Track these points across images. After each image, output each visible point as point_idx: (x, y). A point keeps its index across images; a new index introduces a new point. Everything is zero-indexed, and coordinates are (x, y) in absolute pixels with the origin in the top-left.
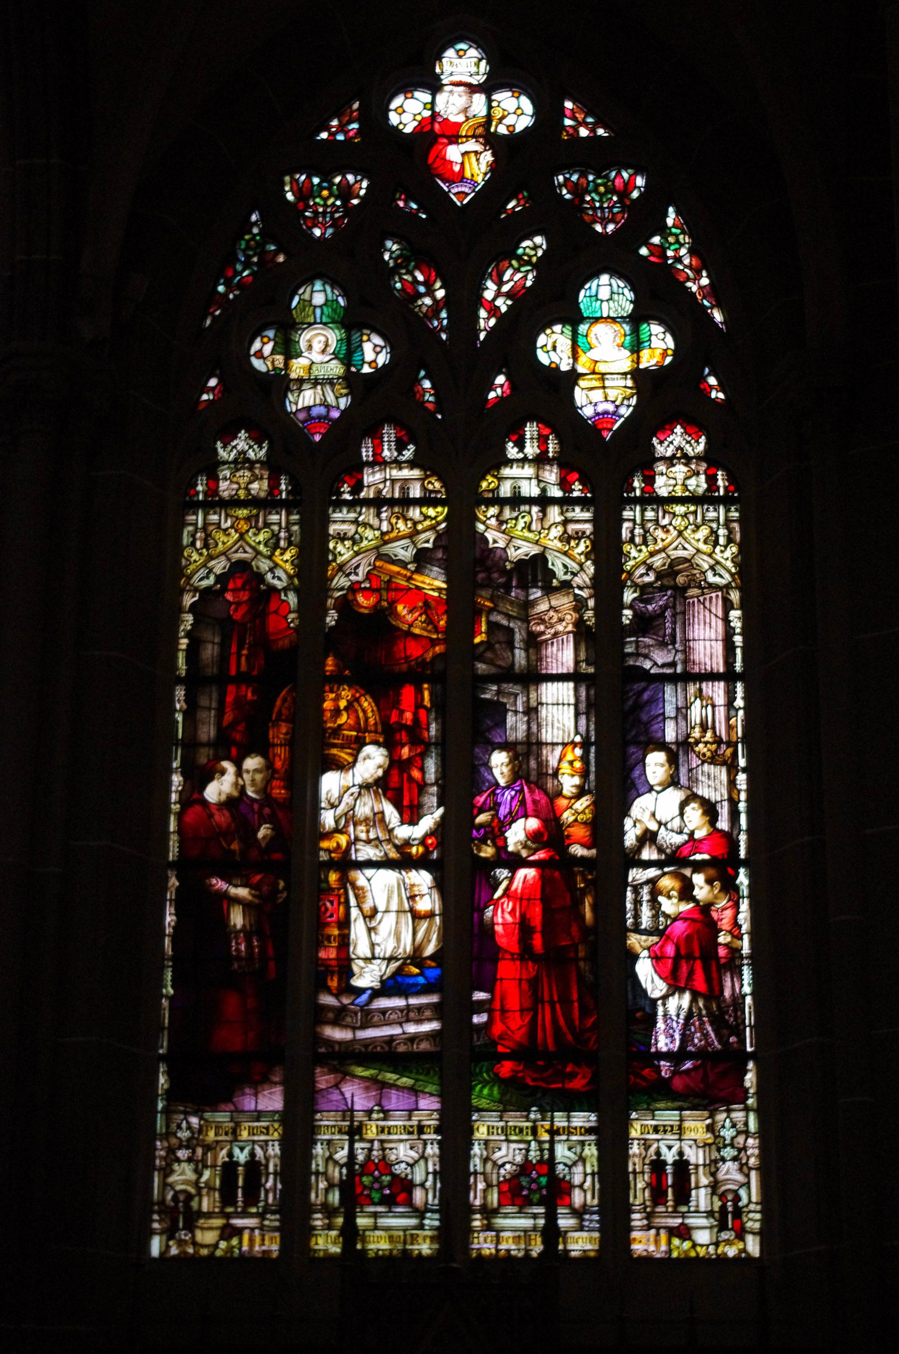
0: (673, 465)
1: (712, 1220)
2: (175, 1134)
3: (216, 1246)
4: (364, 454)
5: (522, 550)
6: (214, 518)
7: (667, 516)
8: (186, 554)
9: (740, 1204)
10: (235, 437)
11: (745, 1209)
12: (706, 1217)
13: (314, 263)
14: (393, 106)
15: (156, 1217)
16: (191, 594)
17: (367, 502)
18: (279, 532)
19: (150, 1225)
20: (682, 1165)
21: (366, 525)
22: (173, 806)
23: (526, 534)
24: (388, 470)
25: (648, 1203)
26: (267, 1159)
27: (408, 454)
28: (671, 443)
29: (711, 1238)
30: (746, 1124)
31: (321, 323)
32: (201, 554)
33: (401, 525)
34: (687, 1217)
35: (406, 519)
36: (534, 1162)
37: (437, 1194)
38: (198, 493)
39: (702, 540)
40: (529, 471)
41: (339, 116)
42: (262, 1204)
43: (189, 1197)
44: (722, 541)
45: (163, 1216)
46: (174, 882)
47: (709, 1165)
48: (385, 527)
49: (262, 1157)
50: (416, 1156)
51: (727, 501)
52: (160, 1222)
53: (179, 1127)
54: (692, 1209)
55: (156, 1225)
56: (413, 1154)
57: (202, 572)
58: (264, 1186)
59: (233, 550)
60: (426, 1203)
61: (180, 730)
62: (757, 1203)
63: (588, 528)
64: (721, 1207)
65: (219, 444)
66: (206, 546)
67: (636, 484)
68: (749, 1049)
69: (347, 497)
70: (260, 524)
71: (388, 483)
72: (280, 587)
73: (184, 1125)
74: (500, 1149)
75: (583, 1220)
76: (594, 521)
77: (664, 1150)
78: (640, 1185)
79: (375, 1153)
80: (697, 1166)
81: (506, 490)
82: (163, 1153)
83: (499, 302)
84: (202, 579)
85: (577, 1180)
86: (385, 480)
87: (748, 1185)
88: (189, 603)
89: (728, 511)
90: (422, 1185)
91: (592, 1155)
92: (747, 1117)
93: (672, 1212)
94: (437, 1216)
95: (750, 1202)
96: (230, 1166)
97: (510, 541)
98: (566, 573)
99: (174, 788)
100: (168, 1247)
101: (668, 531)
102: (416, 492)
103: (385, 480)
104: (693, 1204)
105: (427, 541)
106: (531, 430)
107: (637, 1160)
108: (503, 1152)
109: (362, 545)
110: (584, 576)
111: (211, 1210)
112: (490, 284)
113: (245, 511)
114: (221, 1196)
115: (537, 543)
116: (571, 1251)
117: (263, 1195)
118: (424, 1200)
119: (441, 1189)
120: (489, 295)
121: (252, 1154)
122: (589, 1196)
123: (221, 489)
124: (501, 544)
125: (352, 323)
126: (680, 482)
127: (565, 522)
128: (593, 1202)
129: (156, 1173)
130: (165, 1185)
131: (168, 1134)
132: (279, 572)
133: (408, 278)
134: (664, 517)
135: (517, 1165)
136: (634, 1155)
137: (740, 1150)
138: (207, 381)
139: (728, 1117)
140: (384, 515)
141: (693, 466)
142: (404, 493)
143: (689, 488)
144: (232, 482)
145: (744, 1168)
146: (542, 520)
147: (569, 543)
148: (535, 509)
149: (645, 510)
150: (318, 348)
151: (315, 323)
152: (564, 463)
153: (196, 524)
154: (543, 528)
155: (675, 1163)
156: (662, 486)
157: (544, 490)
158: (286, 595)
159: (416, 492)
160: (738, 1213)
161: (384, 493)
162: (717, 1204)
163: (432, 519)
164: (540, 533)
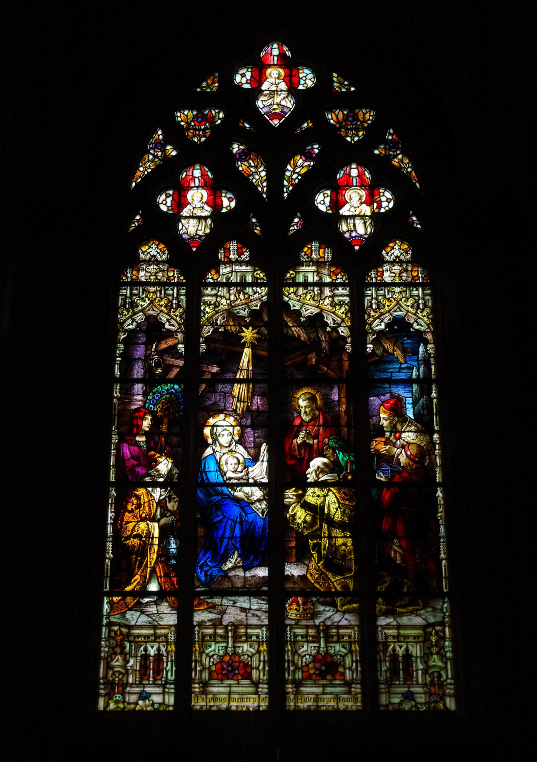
0: (150, 265)
1: (426, 689)
3: (137, 704)
4: (220, 256)
5: (310, 310)
7: (390, 293)
8: (120, 310)
9: (442, 679)
13: (190, 155)
14: (241, 72)
18: (419, 300)
20: (408, 656)
21: (223, 297)
22: (112, 451)
28: (393, 254)
30: (444, 632)
32: (128, 311)
34: (412, 687)
44: (421, 306)
45: (106, 686)
47: (424, 657)
50: (254, 651)
52: (104, 689)
54: (414, 683)
55: (102, 691)
57: (129, 321)
59: (393, 310)
61: (434, 409)
63: (347, 299)
64: (430, 682)
71: (234, 273)
75: (351, 688)
76: (350, 295)
77: (398, 648)
79: (229, 649)
80: (417, 657)
81: (300, 279)
84: (377, 326)
85: (255, 664)
86: (232, 272)
88: (371, 339)
89: (424, 290)
91: (264, 650)
94: (359, 686)
97: (302, 306)
101: (391, 301)
104: (415, 679)
105: (257, 306)
108: (305, 648)
109: (220, 308)
111: (134, 682)
115: (318, 307)
116: (321, 706)
122: (262, 674)
124: (298, 308)
125: (214, 188)
127: (333, 296)
132: (173, 322)
134: (143, 294)
138: (135, 216)
139: (119, 629)
140: (232, 292)
142: (242, 279)
143: (403, 278)
145: (443, 657)
148: (316, 289)
149: (180, 290)
153: (372, 296)
157: (321, 278)
162: (428, 679)
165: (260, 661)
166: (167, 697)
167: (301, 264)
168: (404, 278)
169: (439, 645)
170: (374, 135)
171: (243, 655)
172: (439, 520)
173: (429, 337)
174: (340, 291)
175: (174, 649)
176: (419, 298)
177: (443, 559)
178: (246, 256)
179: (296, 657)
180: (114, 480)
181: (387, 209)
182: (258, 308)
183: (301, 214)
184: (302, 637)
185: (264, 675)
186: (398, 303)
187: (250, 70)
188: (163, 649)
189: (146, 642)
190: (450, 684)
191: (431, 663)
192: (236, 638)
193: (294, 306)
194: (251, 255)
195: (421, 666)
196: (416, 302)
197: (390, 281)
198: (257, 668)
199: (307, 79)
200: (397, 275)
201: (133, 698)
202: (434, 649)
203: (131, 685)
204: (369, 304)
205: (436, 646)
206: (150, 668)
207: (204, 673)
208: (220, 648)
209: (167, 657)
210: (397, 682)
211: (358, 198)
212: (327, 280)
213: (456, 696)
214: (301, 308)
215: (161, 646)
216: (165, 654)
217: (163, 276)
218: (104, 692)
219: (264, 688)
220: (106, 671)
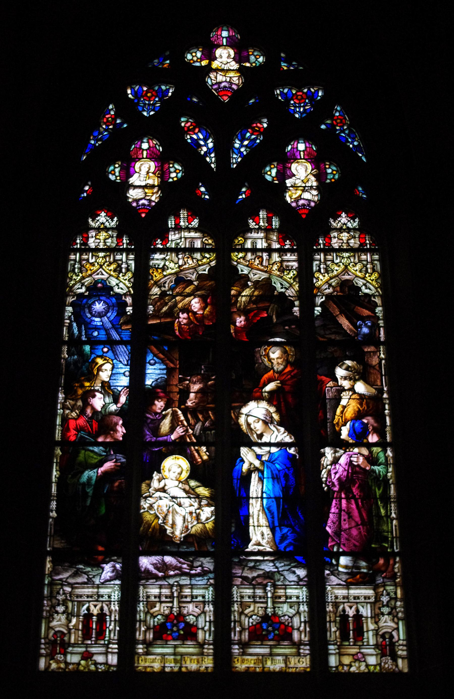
0: (342, 233)
2: (55, 597)
4: (170, 224)
6: (85, 257)
7: (94, 258)
9: (394, 640)
10: (340, 216)
11: (397, 644)
12: (374, 648)
15: (43, 646)
16: (320, 297)
17: (171, 250)
19: (39, 651)
20: (358, 617)
22: (59, 411)
23: (260, 266)
24: (183, 233)
25: (339, 640)
29: (377, 661)
30: (396, 593)
31: (304, 159)
32: (324, 276)
33: (190, 261)
35: (193, 259)
37: (116, 634)
38: (77, 244)
39: (358, 270)
40: (261, 235)
41: (158, 58)
42: (107, 639)
44: (369, 271)
46: (58, 452)
48: (181, 262)
49: (107, 610)
52: (45, 649)
53: (58, 593)
54: (365, 644)
55: (43, 651)
56: (197, 610)
58: (108, 628)
60: (205, 639)
62: (403, 640)
63: (295, 265)
65: (90, 220)
66: (327, 271)
67: (321, 242)
69: (160, 246)
70: (112, 260)
71: (183, 240)
72: (122, 293)
73: (61, 592)
74: (250, 607)
75: (299, 649)
77: (347, 609)
78: (333, 629)
79: (175, 609)
80: (367, 618)
81: (249, 245)
82: (48, 608)
83: (242, 150)
84: (79, 288)
86: (181, 238)
87: (397, 629)
90: (298, 629)
93: (95, 644)
94: (308, 647)
95: (399, 639)
96: (89, 616)
99: (59, 401)
100: (50, 664)
101: (339, 266)
102: (198, 244)
103: (181, 238)
104: (365, 640)
105: (205, 270)
106: (262, 214)
107: (332, 615)
108: (252, 608)
110: (292, 290)
112: (237, 141)
113: (347, 254)
114: (83, 634)
117: (107, 633)
118: (203, 638)
120: (237, 146)
121: (102, 609)
122: (303, 636)
124: (246, 272)
125: (161, 160)
126: (345, 242)
128: (305, 638)
129: (44, 621)
130: (49, 628)
131: (52, 596)
133: (195, 137)
135: (260, 617)
136: (330, 611)
137: (392, 609)
139: (385, 589)
141: (352, 234)
144: (96, 239)
146: (269, 260)
147: (284, 273)
150: (301, 171)
151: (143, 158)
153: (320, 260)
154: (269, 264)
155: (354, 616)
157: (270, 245)
158: (125, 298)
159: (198, 244)
160: (392, 645)
163: (208, 258)
164: (267, 267)
165: (206, 622)
166: (110, 656)
167: (251, 230)
168: (108, 244)
169: (390, 605)
170: (322, 110)
171: (283, 616)
172: (389, 480)
173: (378, 300)
174: (289, 256)
175: (212, 609)
176: (123, 262)
178: (195, 223)
179: (148, 618)
180: (60, 440)
181: (175, 179)
182: (206, 272)
183: (248, 184)
184: (155, 597)
185: (210, 635)
186: (346, 267)
187: (200, 49)
188: (106, 608)
189: (89, 602)
190: (402, 645)
191: (381, 624)
192: (254, 597)
193: (242, 271)
194: (200, 222)
195: (372, 626)
196: (364, 266)
197: (338, 247)
198: (298, 629)
199: (257, 59)
200: (102, 241)
201: (75, 659)
202: (386, 610)
203: (74, 645)
204: (318, 268)
205: (387, 606)
206: (93, 627)
207: (243, 634)
208: (166, 608)
209: (110, 616)
210: (347, 643)
211: (304, 170)
212: (276, 246)
213: (410, 658)
214: (249, 273)
215: (104, 605)
217: (112, 242)
218: (45, 652)
219: (209, 649)
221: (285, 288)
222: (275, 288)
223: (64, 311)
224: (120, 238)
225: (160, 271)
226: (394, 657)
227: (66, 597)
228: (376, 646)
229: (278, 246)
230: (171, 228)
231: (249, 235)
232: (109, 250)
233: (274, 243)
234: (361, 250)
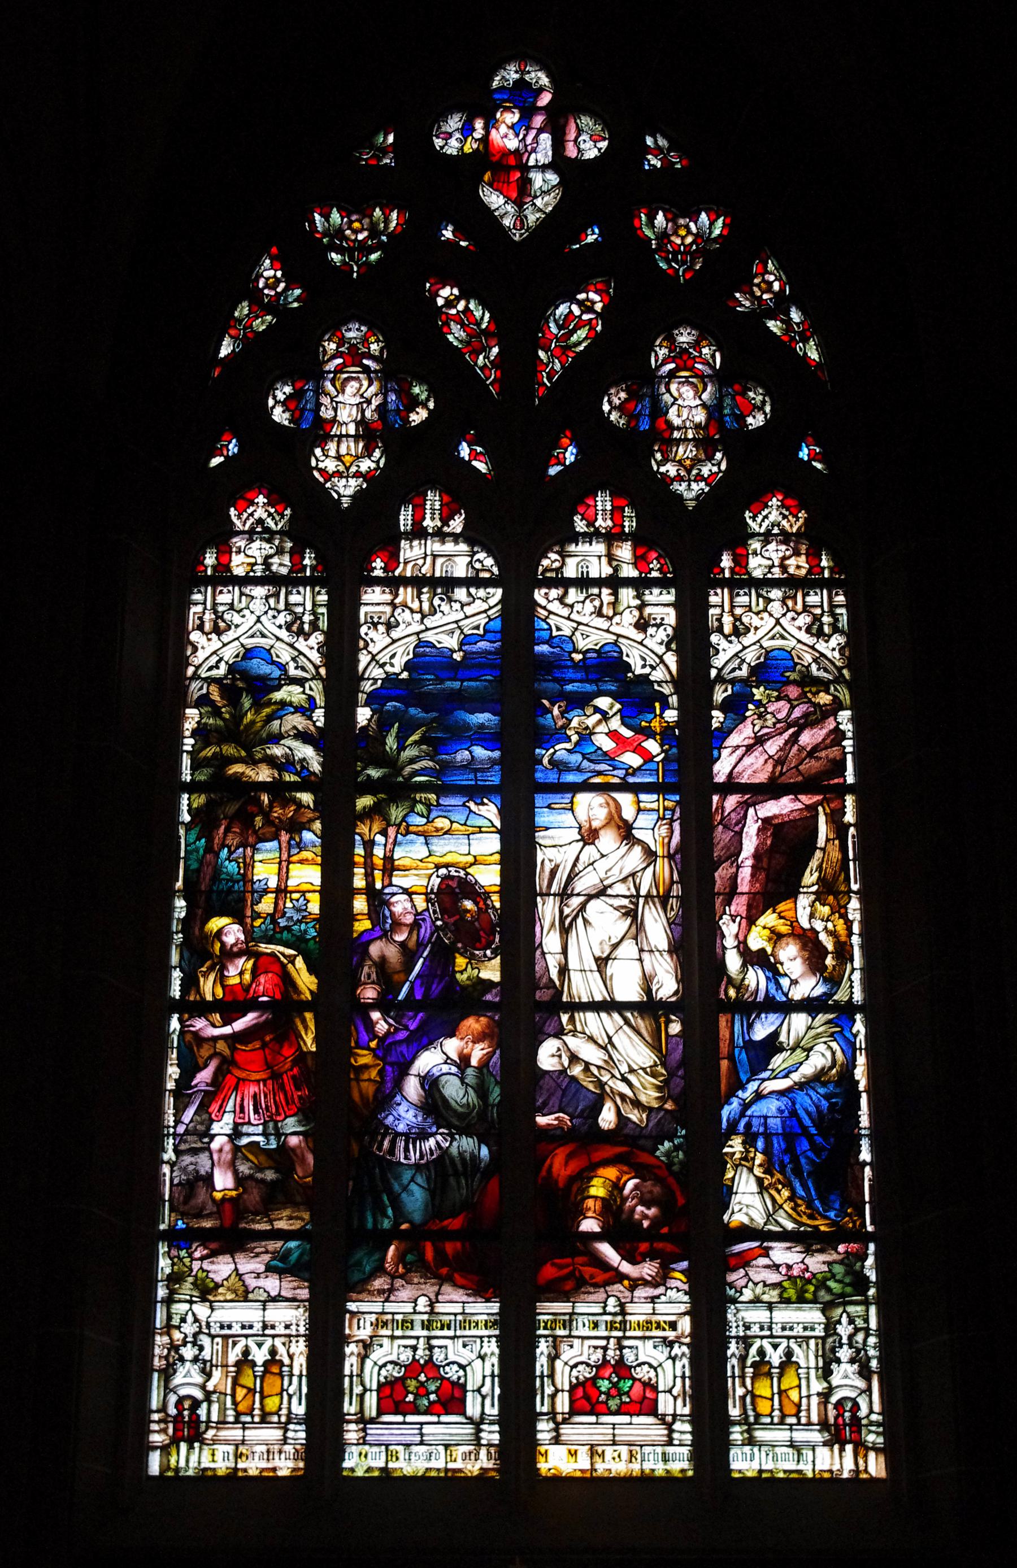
4: (402, 522)
12: (820, 1431)
18: (822, 615)
26: (291, 1357)
27: (457, 525)
36: (422, 1362)
43: (196, 1404)
51: (829, 585)
68: (870, 1228)
69: (378, 573)
70: (799, 607)
71: (429, 559)
75: (286, 1430)
77: (769, 1349)
81: (570, 571)
87: (869, 1390)
88: (720, 699)
91: (492, 1354)
92: (867, 1311)
94: (496, 1428)
95: (871, 1412)
97: (576, 629)
98: (644, 666)
119: (500, 1396)
121: (273, 1352)
123: (233, 564)
125: (392, 374)
126: (260, 561)
128: (493, 1411)
145: (865, 1372)
152: (640, 540)
156: (757, 567)
161: (423, 571)
167: (575, 537)
174: (653, 596)
177: (864, 1164)
188: (282, 1350)
191: (836, 1380)
204: (198, 622)
216: (286, 1361)
220: (165, 1396)
221: (651, 666)
222: (628, 665)
223: (182, 718)
224: (297, 554)
225: (381, 628)
226: (861, 1448)
227: (200, 1327)
228: (824, 1425)
229: (634, 573)
230: (406, 533)
231: (572, 548)
232: (792, 584)
233: (624, 566)
234: (291, 581)
